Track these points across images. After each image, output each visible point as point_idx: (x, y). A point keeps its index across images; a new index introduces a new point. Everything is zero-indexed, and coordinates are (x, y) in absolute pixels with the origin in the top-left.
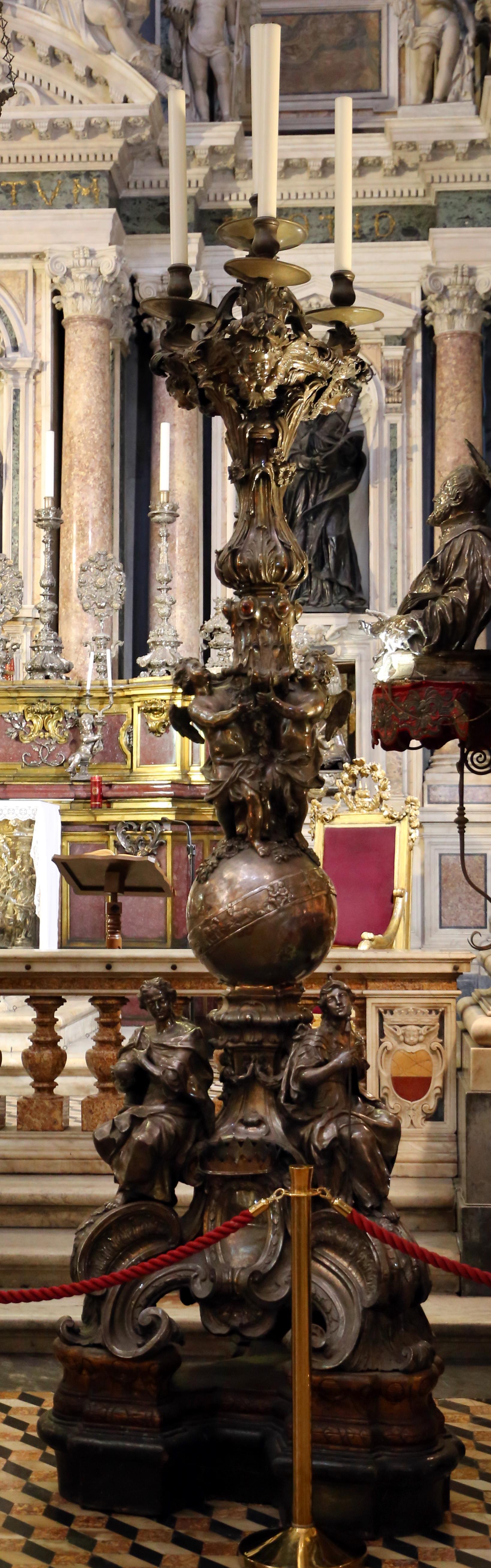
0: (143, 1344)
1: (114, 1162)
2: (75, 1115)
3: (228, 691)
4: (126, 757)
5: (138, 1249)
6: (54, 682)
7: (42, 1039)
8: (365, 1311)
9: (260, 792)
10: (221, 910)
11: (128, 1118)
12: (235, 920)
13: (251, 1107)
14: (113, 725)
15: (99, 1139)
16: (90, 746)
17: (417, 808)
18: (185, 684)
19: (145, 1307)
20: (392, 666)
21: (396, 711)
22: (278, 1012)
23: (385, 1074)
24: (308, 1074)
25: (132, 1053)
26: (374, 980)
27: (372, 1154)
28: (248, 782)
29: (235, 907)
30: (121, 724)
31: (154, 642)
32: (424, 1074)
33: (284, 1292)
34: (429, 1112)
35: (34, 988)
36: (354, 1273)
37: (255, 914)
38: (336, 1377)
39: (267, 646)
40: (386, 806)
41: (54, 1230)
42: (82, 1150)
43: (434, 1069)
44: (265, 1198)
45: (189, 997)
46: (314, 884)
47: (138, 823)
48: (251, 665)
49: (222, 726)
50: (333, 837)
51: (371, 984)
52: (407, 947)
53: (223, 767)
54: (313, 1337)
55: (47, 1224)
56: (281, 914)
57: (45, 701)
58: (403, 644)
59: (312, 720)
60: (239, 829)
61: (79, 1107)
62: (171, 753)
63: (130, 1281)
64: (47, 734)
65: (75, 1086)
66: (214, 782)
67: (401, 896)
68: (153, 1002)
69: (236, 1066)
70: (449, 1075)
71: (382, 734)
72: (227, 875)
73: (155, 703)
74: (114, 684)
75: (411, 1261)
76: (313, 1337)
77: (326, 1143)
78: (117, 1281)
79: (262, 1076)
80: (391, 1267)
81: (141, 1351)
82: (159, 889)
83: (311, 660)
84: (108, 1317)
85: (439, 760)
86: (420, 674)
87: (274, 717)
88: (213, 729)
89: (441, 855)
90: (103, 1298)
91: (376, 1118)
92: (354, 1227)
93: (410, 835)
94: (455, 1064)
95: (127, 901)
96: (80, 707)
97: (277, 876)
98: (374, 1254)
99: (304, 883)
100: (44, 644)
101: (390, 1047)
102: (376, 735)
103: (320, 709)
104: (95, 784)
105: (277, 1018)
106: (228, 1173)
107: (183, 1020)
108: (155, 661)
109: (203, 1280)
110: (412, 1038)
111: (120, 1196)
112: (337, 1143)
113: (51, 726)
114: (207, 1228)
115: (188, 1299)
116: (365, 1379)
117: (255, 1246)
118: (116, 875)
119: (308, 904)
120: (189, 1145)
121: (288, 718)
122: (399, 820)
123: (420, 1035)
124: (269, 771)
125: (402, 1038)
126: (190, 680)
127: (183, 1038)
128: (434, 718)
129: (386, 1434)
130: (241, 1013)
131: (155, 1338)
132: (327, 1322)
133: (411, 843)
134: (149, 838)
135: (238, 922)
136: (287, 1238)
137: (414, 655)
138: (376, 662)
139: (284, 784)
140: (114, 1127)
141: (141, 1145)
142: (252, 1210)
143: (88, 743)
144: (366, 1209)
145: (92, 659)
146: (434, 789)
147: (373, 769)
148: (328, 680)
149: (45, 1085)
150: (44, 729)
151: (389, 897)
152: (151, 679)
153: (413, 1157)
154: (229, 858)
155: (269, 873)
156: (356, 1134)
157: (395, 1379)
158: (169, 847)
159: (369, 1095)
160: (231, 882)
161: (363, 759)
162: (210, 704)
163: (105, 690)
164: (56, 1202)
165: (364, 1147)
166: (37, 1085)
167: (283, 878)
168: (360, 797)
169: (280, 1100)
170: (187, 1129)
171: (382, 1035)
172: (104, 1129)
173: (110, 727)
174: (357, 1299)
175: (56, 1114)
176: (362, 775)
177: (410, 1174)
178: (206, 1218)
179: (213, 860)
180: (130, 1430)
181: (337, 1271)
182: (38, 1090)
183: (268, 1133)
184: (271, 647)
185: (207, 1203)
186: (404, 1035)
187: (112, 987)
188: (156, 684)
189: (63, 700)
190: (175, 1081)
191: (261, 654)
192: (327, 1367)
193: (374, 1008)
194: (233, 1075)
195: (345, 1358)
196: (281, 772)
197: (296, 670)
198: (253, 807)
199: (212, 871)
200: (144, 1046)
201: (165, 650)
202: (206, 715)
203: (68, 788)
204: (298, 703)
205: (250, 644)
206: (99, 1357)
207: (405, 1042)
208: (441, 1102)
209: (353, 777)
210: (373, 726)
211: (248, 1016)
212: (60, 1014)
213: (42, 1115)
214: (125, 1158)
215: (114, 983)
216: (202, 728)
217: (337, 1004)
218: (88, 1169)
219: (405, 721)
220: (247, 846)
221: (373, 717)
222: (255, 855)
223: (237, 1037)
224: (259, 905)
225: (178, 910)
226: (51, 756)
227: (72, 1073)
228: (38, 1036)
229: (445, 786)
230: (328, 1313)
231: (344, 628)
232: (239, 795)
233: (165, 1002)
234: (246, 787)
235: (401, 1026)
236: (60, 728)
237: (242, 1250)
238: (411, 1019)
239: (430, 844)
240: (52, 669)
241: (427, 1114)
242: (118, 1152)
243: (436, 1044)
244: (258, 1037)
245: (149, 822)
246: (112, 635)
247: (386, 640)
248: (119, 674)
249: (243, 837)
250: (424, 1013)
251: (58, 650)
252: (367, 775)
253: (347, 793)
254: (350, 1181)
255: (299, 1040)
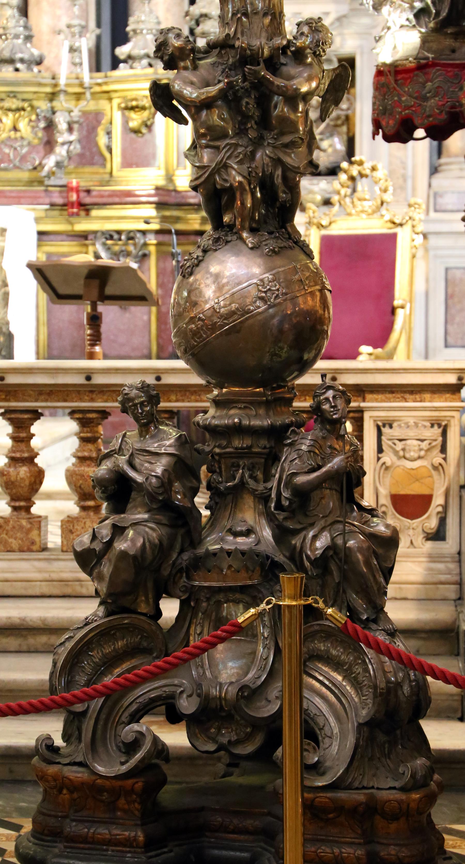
0: (127, 762)
1: (95, 574)
2: (54, 537)
3: (213, 64)
4: (105, 159)
5: (122, 664)
6: (24, 74)
7: (18, 455)
8: (360, 725)
9: (249, 177)
10: (208, 306)
11: (109, 527)
12: (222, 316)
13: (240, 516)
14: (90, 125)
15: (78, 549)
16: (66, 147)
17: (421, 211)
18: (166, 58)
19: (129, 723)
20: (395, 47)
21: (400, 96)
22: (268, 416)
23: (383, 492)
24: (301, 479)
25: (113, 459)
26: (372, 392)
27: (368, 563)
28: (236, 167)
29: (222, 303)
30: (99, 123)
31: (134, 31)
32: (425, 491)
33: (274, 708)
34: (429, 531)
35: (8, 400)
36: (348, 688)
37: (244, 310)
38: (329, 795)
39: (256, 13)
40: (387, 210)
41: (34, 655)
42: (61, 572)
43: (436, 485)
44: (254, 608)
45: (175, 410)
46: (307, 278)
47: (119, 232)
48: (239, 35)
49: (207, 104)
50: (329, 243)
51: (368, 396)
52: (408, 357)
53: (209, 150)
54: (305, 753)
55: (25, 648)
56: (271, 311)
57: (15, 97)
58: (408, 19)
59: (306, 97)
60: (226, 219)
61: (59, 531)
62: (154, 156)
63: (113, 695)
64: (18, 134)
65: (56, 505)
66: (198, 167)
67: (403, 307)
68: (135, 405)
69: (224, 473)
70: (451, 493)
71: (383, 123)
72: (214, 269)
73: (136, 99)
74: (91, 78)
75: (409, 675)
76: (305, 753)
77: (319, 552)
78: (99, 694)
79: (252, 483)
80: (388, 682)
81: (124, 768)
82: (142, 298)
83: (305, 29)
84: (90, 735)
85: (447, 164)
86: (426, 54)
87: (264, 93)
88: (199, 107)
89: (447, 270)
90: (84, 713)
91: (372, 527)
92: (349, 638)
93: (413, 240)
94: (459, 481)
95: (109, 312)
96: (55, 103)
97: (268, 270)
98: (370, 667)
99: (297, 277)
100: (13, 31)
101: (389, 463)
102: (377, 125)
103: (314, 84)
104: (72, 189)
105: (267, 422)
106: (214, 584)
107: (167, 425)
108: (135, 52)
109: (190, 696)
110: (412, 454)
111: (102, 609)
112: (331, 553)
113: (23, 125)
114: (194, 641)
115: (174, 717)
116: (360, 797)
117: (244, 661)
118: (96, 283)
119: (300, 300)
120: (175, 556)
121: (279, 95)
122: (401, 225)
123: (421, 450)
124: (258, 155)
125: (401, 453)
126: (172, 53)
127: (168, 443)
128: (441, 103)
129: (382, 854)
130: (230, 417)
131: (139, 756)
132: (320, 738)
133: (414, 250)
134: (131, 248)
135: (226, 319)
136: (278, 651)
137: (420, 32)
138: (377, 41)
139: (275, 168)
140: (94, 537)
141: (124, 554)
142: (240, 620)
143: (63, 144)
144: (361, 621)
145: (66, 48)
146: (441, 196)
147: (374, 169)
148: (324, 51)
149: (22, 504)
150: (15, 129)
151: (390, 309)
152: (131, 72)
153: (413, 578)
154: (216, 250)
155: (259, 266)
156: (351, 543)
157: (392, 797)
158: (153, 259)
159: (365, 503)
160: (217, 277)
161: (363, 158)
162: (195, 80)
163: (81, 85)
164: (35, 625)
165: (360, 557)
166: (13, 504)
167: (274, 272)
168: (360, 200)
169: (270, 507)
170: (172, 539)
171: (380, 450)
172: (84, 540)
173: (88, 125)
174: (352, 714)
175: (34, 534)
176: (362, 175)
177: (410, 596)
178: (192, 631)
179: (199, 253)
180: (113, 851)
181: (330, 685)
182: (15, 509)
183: (258, 542)
184: (261, 14)
185: (194, 615)
186: (404, 450)
187: (92, 400)
188: (136, 78)
189: (35, 96)
190: (159, 488)
191: (250, 23)
192: (320, 784)
193: (372, 422)
194: (221, 482)
195: (338, 775)
196: (272, 155)
197: (289, 41)
198: (242, 194)
199: (197, 265)
200: (125, 452)
201: (146, 40)
202: (190, 93)
203: (43, 194)
204: (290, 78)
205: (238, 11)
206: (79, 775)
207: (405, 457)
208: (443, 521)
209: (352, 179)
210: (373, 114)
211: (236, 420)
212: (35, 428)
213: (19, 535)
214: (106, 568)
215: (94, 396)
216: (186, 107)
217: (332, 407)
218: (68, 591)
219: (408, 108)
220: (235, 237)
221: (374, 104)
222: (243, 247)
223: (225, 443)
224: (248, 301)
225: (163, 327)
226: (23, 158)
227: (49, 496)
228: (14, 452)
229: (453, 192)
230: (321, 729)
231: (345, 16)
232: (226, 181)
233: (148, 406)
234: (234, 172)
235: (400, 440)
236: (33, 127)
237: (230, 664)
238: (411, 433)
239: (436, 256)
240: (22, 61)
241: (428, 534)
242: (99, 562)
243: (438, 459)
244: (247, 442)
245: (130, 232)
246: (87, 21)
247: (389, 15)
248: (97, 67)
249: (231, 227)
250: (425, 427)
251: (29, 38)
252: (367, 176)
253: (345, 196)
254: (344, 592)
255: (291, 445)
